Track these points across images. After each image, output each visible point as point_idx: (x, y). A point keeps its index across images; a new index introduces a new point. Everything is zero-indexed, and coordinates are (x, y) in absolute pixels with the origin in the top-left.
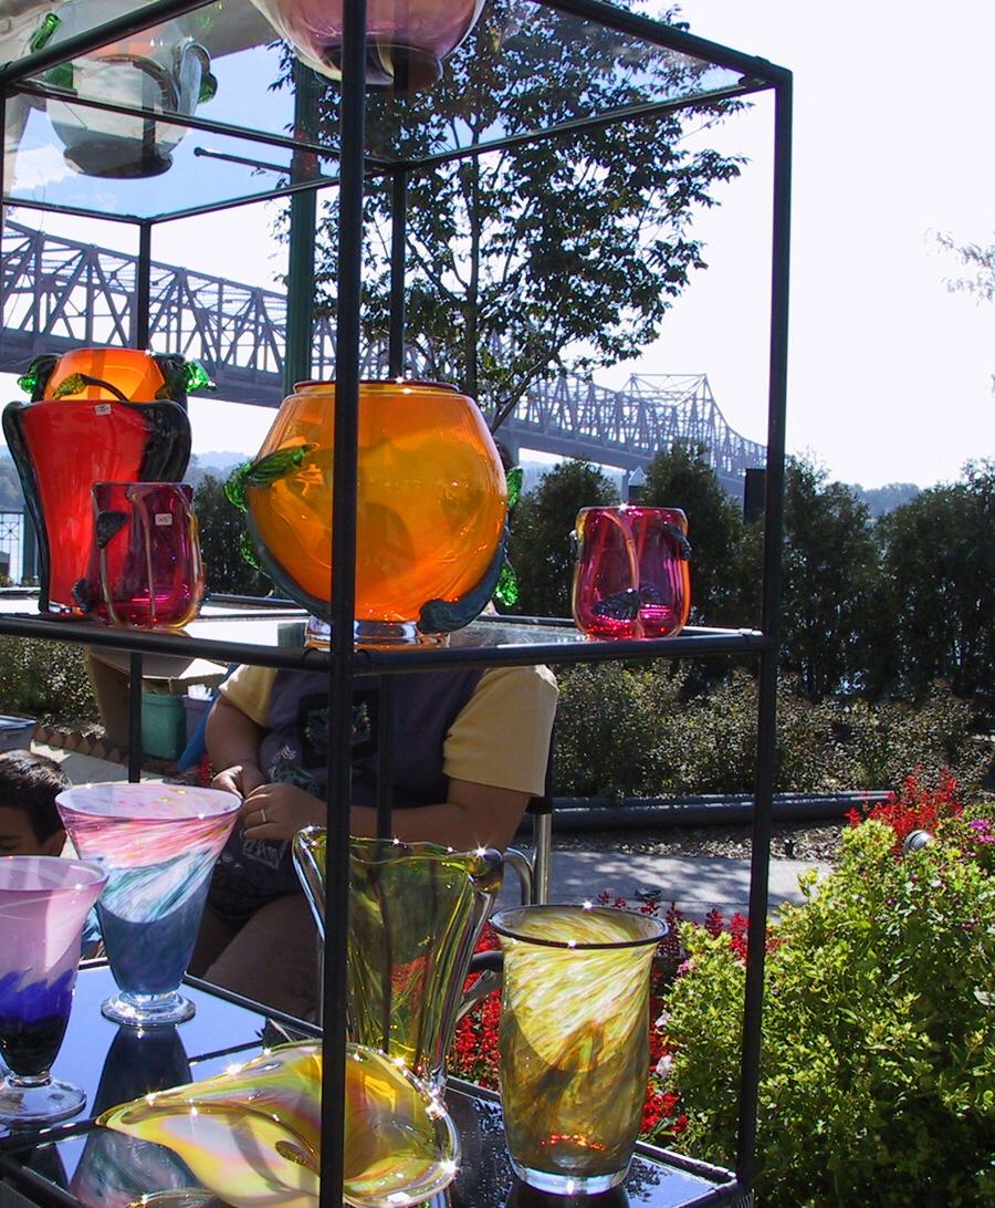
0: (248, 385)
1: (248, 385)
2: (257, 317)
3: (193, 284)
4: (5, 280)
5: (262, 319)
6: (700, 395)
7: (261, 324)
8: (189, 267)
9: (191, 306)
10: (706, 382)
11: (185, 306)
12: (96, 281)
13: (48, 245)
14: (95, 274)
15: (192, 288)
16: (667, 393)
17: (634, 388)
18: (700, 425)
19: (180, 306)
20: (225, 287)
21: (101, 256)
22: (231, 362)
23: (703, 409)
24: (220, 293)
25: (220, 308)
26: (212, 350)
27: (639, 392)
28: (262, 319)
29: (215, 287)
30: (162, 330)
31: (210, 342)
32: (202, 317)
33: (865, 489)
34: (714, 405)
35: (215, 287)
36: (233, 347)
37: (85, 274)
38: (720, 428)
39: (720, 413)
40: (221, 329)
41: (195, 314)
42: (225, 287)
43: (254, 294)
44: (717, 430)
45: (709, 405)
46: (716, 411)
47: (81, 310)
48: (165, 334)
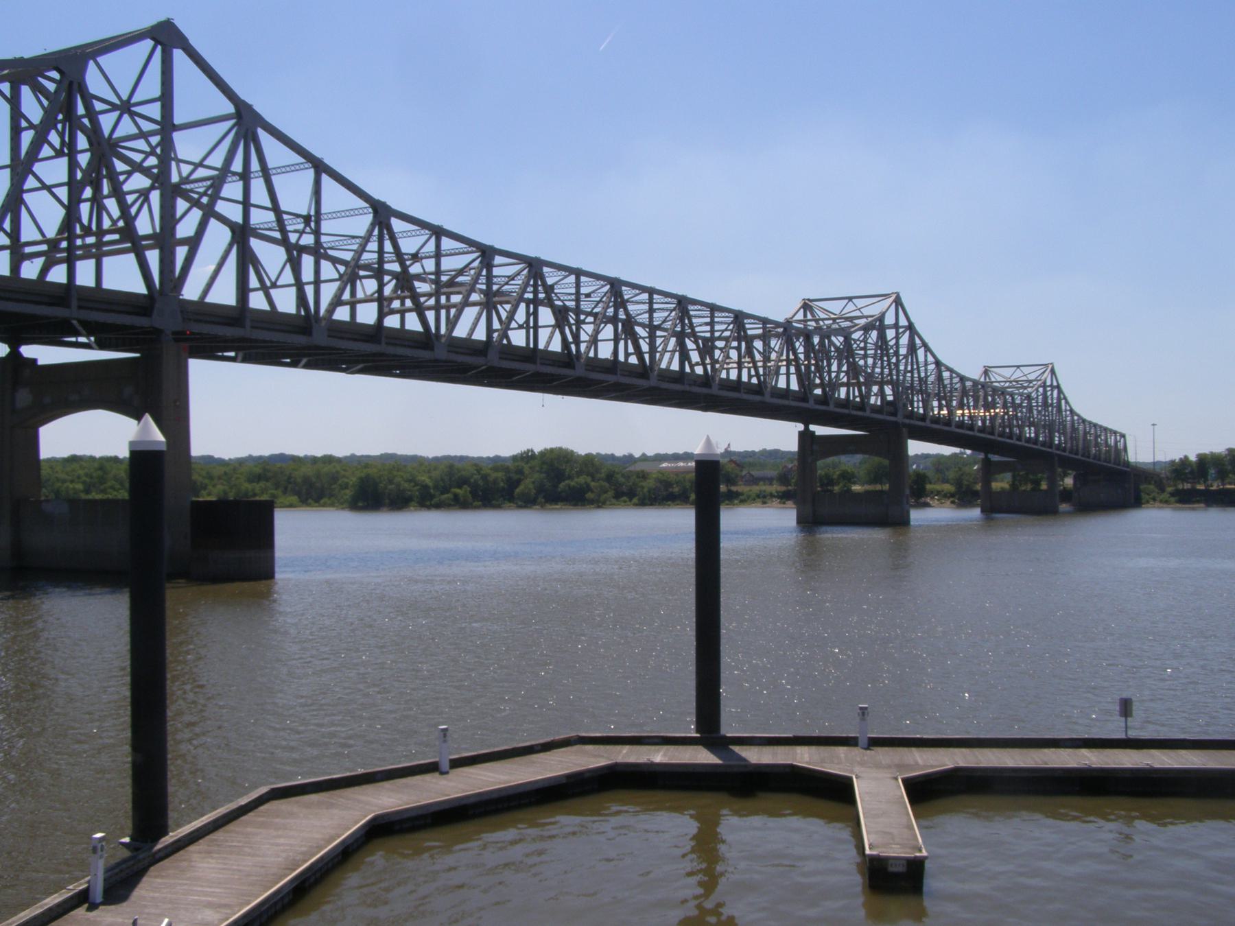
0: (677, 387)
1: (677, 387)
2: (616, 312)
3: (627, 293)
4: (121, 228)
5: (622, 316)
6: (1048, 383)
7: (621, 320)
8: (691, 295)
9: (549, 303)
10: (1053, 372)
11: (542, 303)
12: (792, 357)
13: (498, 260)
14: (540, 288)
15: (550, 281)
16: (1017, 382)
17: (809, 316)
18: (1050, 408)
19: (536, 302)
20: (583, 279)
21: (545, 269)
22: (592, 354)
23: (1052, 394)
24: (651, 302)
25: (578, 305)
26: (573, 347)
27: (817, 321)
28: (622, 316)
29: (645, 296)
30: (520, 327)
31: (570, 339)
32: (561, 315)
33: (817, 434)
34: (1060, 391)
35: (645, 296)
36: (594, 341)
37: (530, 289)
38: (926, 364)
39: (925, 345)
40: (579, 323)
41: (554, 313)
42: (583, 279)
43: (974, 382)
44: (1064, 413)
45: (1055, 392)
46: (918, 341)
47: (521, 323)
48: (524, 331)
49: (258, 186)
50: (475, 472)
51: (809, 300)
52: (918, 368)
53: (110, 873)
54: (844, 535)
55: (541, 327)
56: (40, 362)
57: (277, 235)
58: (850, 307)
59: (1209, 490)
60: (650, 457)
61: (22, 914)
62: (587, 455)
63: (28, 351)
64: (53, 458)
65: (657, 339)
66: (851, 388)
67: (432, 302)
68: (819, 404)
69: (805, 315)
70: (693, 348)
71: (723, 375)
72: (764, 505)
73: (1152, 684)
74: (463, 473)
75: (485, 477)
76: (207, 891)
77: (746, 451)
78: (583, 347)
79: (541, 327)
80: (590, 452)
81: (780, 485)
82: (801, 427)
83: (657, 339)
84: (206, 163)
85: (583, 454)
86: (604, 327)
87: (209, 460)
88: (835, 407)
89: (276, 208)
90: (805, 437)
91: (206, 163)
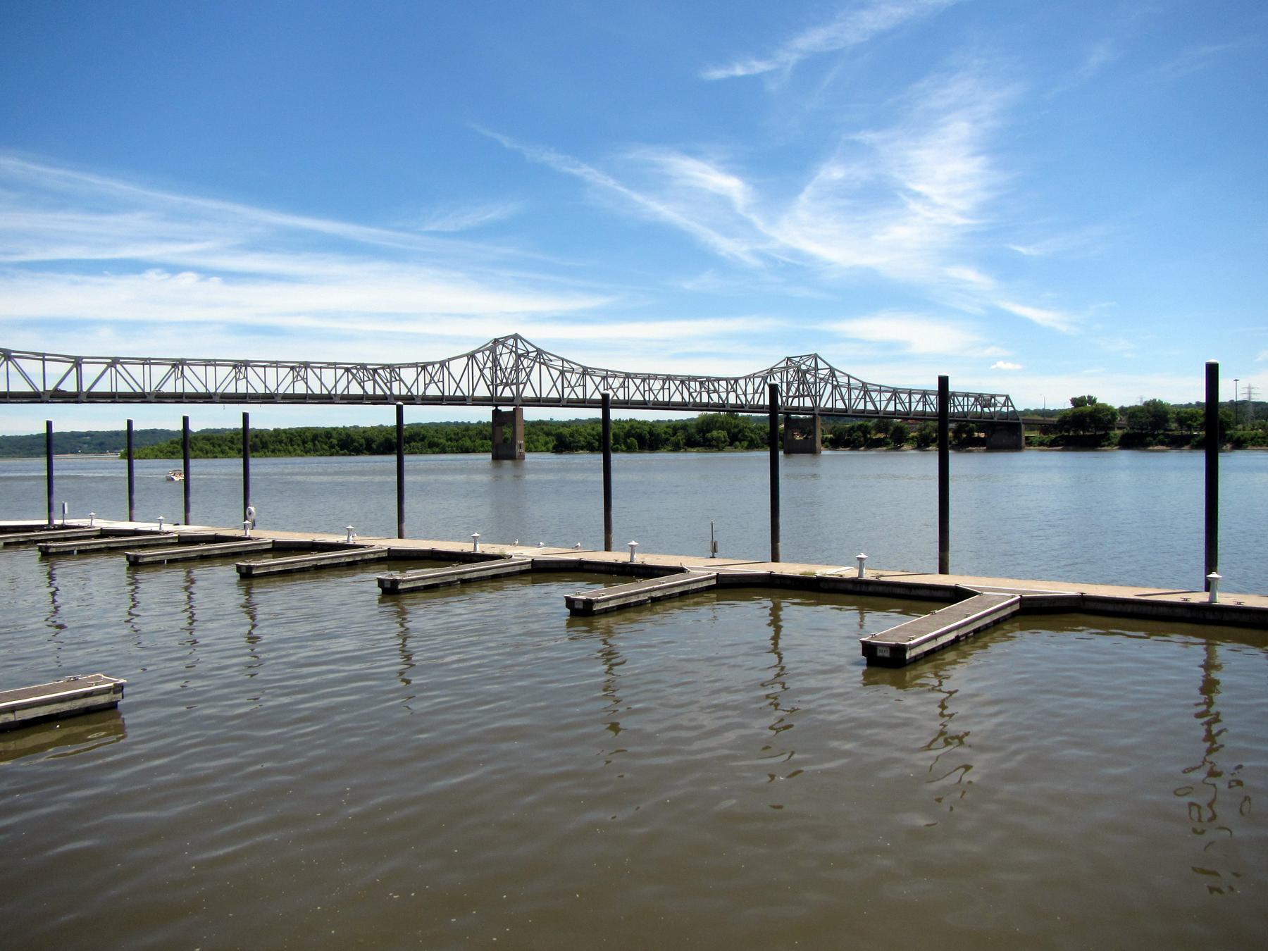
54: (761, 455)
55: (8, 389)
59: (1206, 695)
60: (473, 424)
61: (519, 723)
62: (275, 430)
63: (499, 408)
65: (377, 393)
66: (470, 394)
77: (31, 435)
78: (749, 397)
79: (8, 389)
80: (1105, 402)
81: (561, 433)
83: (377, 393)
84: (597, 384)
85: (195, 431)
86: (344, 391)
87: (1222, 403)
90: (496, 413)
91: (597, 384)
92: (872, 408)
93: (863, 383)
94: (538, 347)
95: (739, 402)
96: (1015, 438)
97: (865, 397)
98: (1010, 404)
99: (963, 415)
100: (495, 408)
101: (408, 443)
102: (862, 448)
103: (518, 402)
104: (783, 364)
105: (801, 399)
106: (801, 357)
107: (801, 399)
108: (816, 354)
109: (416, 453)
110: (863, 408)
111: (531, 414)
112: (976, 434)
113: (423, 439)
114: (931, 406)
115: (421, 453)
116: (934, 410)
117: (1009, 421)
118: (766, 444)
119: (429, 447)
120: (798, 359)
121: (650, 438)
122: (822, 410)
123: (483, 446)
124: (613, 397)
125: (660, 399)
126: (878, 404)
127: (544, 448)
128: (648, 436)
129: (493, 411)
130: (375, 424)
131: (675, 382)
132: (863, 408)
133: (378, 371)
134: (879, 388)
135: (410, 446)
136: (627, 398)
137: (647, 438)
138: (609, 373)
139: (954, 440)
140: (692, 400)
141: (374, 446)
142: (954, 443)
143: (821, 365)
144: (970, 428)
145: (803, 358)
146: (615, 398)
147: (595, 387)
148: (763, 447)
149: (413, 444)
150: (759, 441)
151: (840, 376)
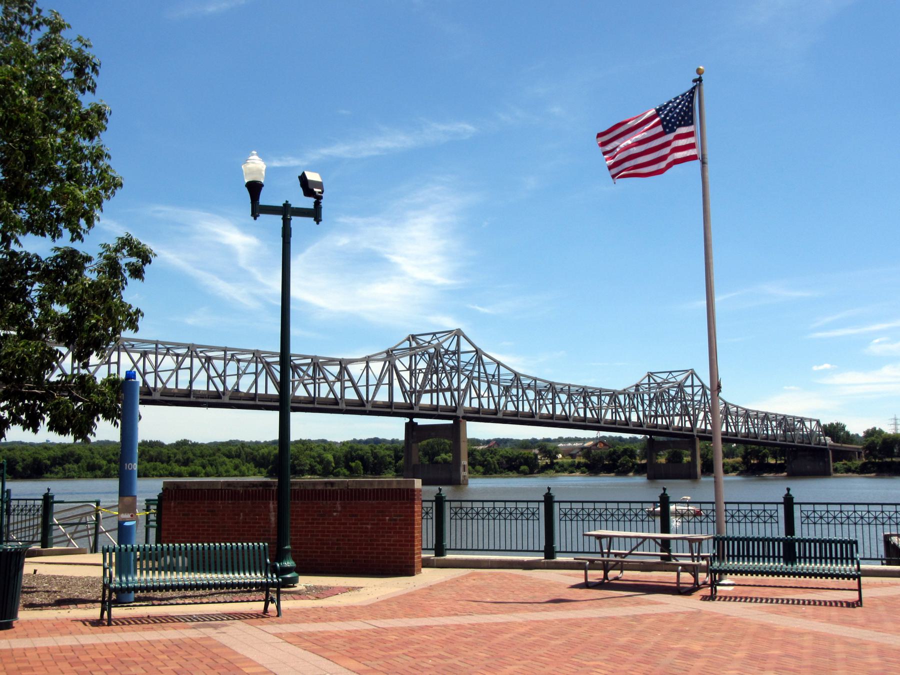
33: (419, 424)
49: (482, 367)
50: (370, 452)
51: (650, 373)
52: (708, 401)
53: (630, 643)
56: (419, 424)
57: (486, 379)
58: (670, 376)
63: (415, 420)
64: (157, 441)
67: (578, 398)
68: (144, 395)
69: (649, 381)
70: (227, 384)
71: (467, 404)
72: (571, 474)
73: (710, 667)
74: (360, 452)
75: (375, 456)
76: (575, 661)
82: (408, 420)
84: (136, 361)
88: (346, 406)
89: (485, 373)
90: (411, 428)
91: (136, 361)
92: (355, 397)
93: (516, 375)
94: (478, 345)
95: (212, 388)
96: (821, 464)
97: (694, 412)
98: (347, 377)
99: (754, 436)
100: (408, 420)
101: (61, 464)
102: (631, 474)
103: (460, 413)
104: (406, 345)
105: (435, 395)
106: (434, 334)
107: (435, 395)
108: (459, 330)
109: (73, 477)
110: (387, 400)
111: (476, 431)
112: (752, 462)
113: (77, 461)
114: (593, 411)
115: (79, 477)
116: (596, 417)
117: (770, 441)
118: (505, 469)
119: (88, 470)
120: (428, 338)
121: (373, 461)
122: (466, 411)
123: (155, 469)
124: (328, 394)
125: (171, 385)
126: (363, 391)
127: (236, 472)
128: (371, 459)
129: (406, 424)
130: (235, 439)
131: (132, 354)
132: (387, 400)
133: (214, 361)
134: (154, 346)
135: (64, 469)
136: (435, 403)
137: (370, 461)
138: (160, 346)
139: (536, 455)
140: (160, 385)
141: (19, 468)
142: (741, 469)
143: (465, 346)
144: (764, 453)
145: (438, 335)
146: (576, 415)
147: (132, 365)
148: (501, 472)
149: (67, 466)
150: (497, 466)
151: (489, 363)
